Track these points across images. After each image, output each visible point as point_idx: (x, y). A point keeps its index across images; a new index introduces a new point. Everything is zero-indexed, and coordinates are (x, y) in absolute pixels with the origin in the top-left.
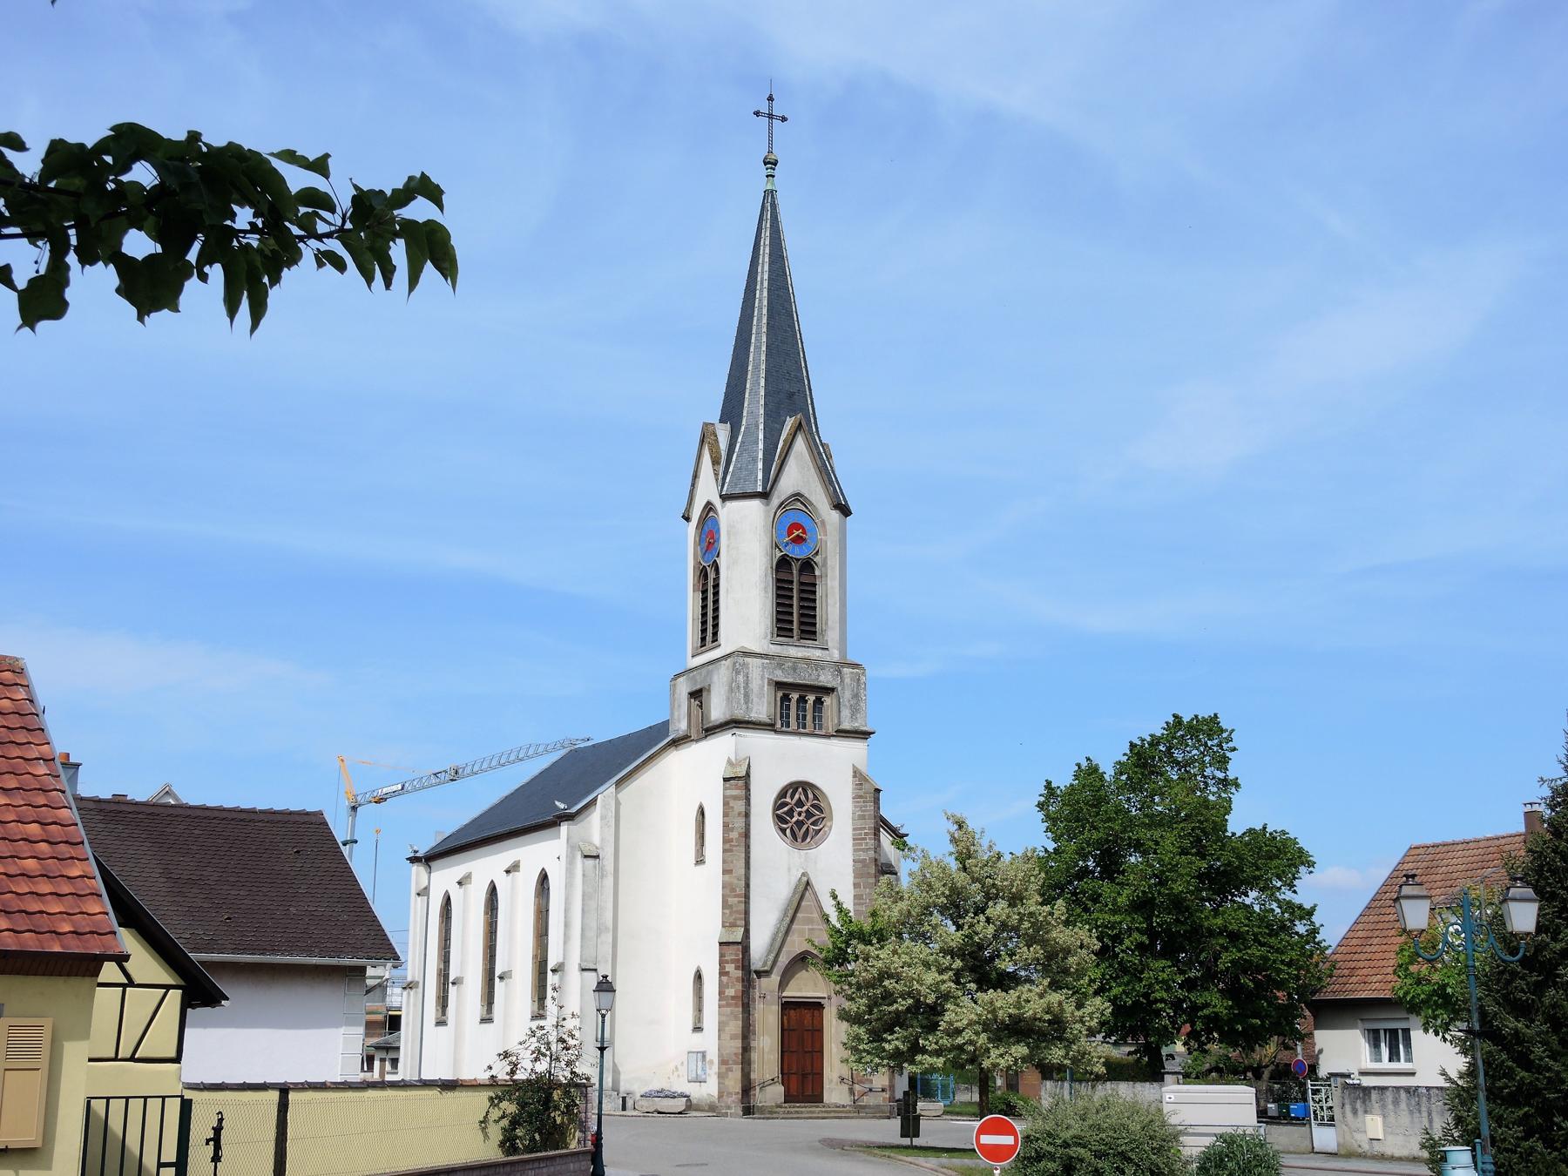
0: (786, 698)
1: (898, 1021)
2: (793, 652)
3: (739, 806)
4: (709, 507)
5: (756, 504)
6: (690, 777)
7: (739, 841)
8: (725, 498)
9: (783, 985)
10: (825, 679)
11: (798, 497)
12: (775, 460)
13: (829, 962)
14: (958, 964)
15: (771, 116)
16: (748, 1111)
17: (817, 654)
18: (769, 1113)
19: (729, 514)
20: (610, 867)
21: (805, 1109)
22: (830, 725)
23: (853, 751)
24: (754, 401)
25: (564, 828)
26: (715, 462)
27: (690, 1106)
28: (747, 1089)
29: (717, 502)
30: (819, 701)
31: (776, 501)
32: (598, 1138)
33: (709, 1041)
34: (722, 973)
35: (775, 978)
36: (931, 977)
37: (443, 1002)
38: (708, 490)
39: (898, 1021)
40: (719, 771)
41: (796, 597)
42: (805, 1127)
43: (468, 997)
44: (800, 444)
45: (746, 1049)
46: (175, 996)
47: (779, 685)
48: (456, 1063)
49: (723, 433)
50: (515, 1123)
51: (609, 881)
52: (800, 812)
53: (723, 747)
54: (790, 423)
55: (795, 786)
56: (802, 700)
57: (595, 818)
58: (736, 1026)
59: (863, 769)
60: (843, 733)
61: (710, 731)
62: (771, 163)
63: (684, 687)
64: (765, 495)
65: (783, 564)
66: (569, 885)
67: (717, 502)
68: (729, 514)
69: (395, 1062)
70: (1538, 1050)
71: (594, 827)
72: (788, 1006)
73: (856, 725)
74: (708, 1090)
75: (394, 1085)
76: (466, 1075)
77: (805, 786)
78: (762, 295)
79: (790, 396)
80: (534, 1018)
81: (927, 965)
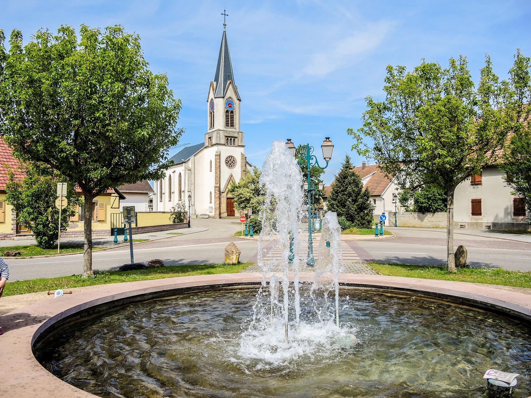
0: (228, 139)
1: (243, 202)
2: (229, 130)
3: (218, 160)
4: (212, 99)
5: (221, 99)
6: (208, 155)
7: (218, 168)
8: (215, 98)
9: (227, 195)
10: (236, 135)
11: (230, 98)
12: (225, 90)
13: (231, 192)
14: (254, 192)
15: (225, 15)
16: (220, 218)
17: (234, 130)
18: (224, 218)
19: (216, 101)
20: (193, 172)
21: (231, 217)
22: (236, 144)
23: (241, 150)
24: (221, 77)
25: (184, 164)
26: (213, 90)
27: (209, 217)
28: (220, 214)
29: (214, 98)
30: (234, 140)
31: (225, 98)
32: (189, 221)
33: (213, 205)
34: (215, 192)
35: (225, 193)
36: (249, 194)
37: (161, 197)
38: (212, 96)
39: (243, 202)
40: (214, 154)
41: (230, 120)
42: (231, 220)
43: (166, 196)
44: (231, 85)
45: (220, 207)
46: (118, 198)
47: (226, 136)
48: (132, 261)
49: (215, 83)
50: (175, 218)
51: (193, 175)
52: (230, 162)
53: (215, 148)
54: (229, 82)
55: (229, 157)
56: (231, 139)
57: (190, 162)
58: (218, 202)
59: (243, 153)
60: (239, 146)
61: (212, 145)
62: (225, 25)
63: (207, 136)
64: (223, 97)
65: (227, 111)
66: (185, 176)
67: (214, 98)
68: (216, 101)
69: (152, 209)
70: (335, 206)
71: (190, 164)
72: (228, 199)
73: (242, 144)
74: (212, 214)
75: (153, 212)
76: (166, 211)
77: (231, 156)
78: (223, 54)
79: (229, 76)
80: (179, 200)
81: (248, 192)
